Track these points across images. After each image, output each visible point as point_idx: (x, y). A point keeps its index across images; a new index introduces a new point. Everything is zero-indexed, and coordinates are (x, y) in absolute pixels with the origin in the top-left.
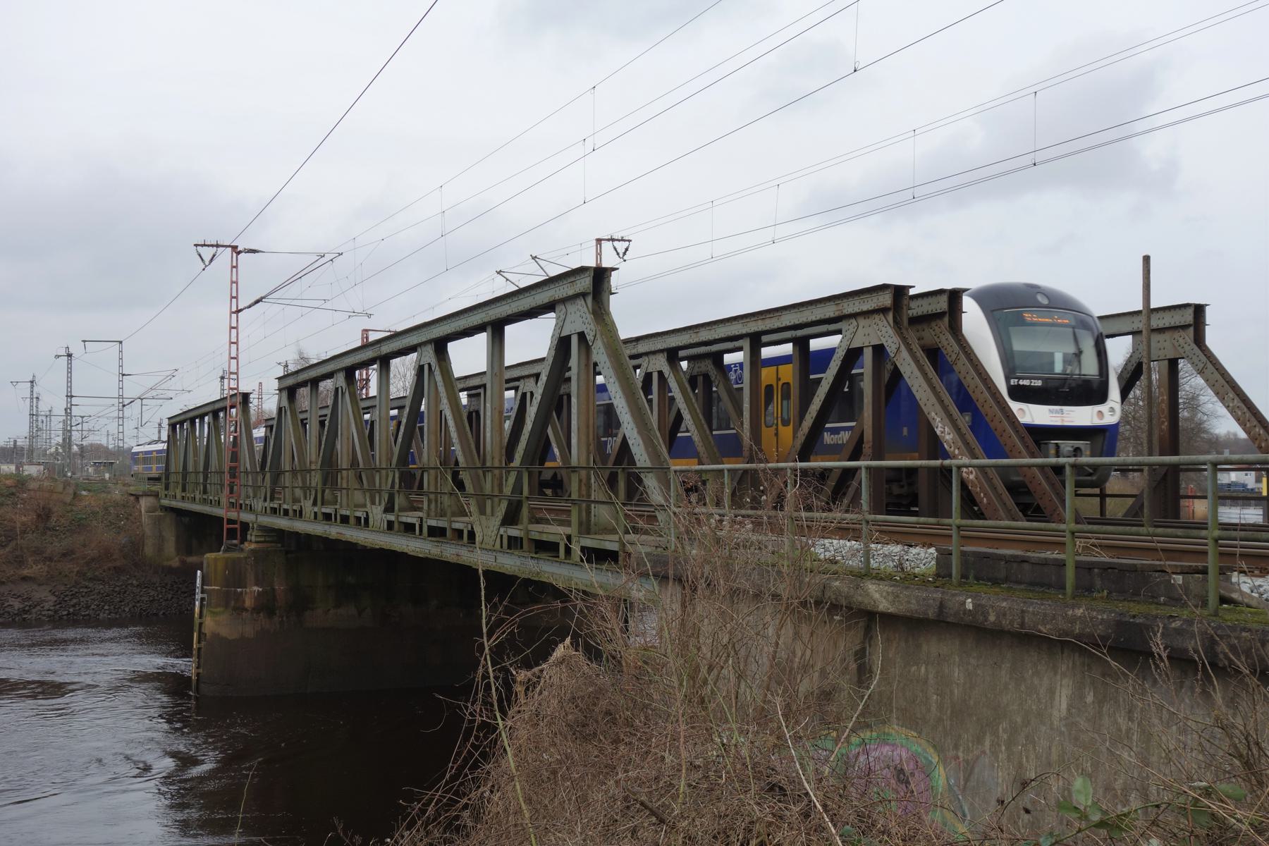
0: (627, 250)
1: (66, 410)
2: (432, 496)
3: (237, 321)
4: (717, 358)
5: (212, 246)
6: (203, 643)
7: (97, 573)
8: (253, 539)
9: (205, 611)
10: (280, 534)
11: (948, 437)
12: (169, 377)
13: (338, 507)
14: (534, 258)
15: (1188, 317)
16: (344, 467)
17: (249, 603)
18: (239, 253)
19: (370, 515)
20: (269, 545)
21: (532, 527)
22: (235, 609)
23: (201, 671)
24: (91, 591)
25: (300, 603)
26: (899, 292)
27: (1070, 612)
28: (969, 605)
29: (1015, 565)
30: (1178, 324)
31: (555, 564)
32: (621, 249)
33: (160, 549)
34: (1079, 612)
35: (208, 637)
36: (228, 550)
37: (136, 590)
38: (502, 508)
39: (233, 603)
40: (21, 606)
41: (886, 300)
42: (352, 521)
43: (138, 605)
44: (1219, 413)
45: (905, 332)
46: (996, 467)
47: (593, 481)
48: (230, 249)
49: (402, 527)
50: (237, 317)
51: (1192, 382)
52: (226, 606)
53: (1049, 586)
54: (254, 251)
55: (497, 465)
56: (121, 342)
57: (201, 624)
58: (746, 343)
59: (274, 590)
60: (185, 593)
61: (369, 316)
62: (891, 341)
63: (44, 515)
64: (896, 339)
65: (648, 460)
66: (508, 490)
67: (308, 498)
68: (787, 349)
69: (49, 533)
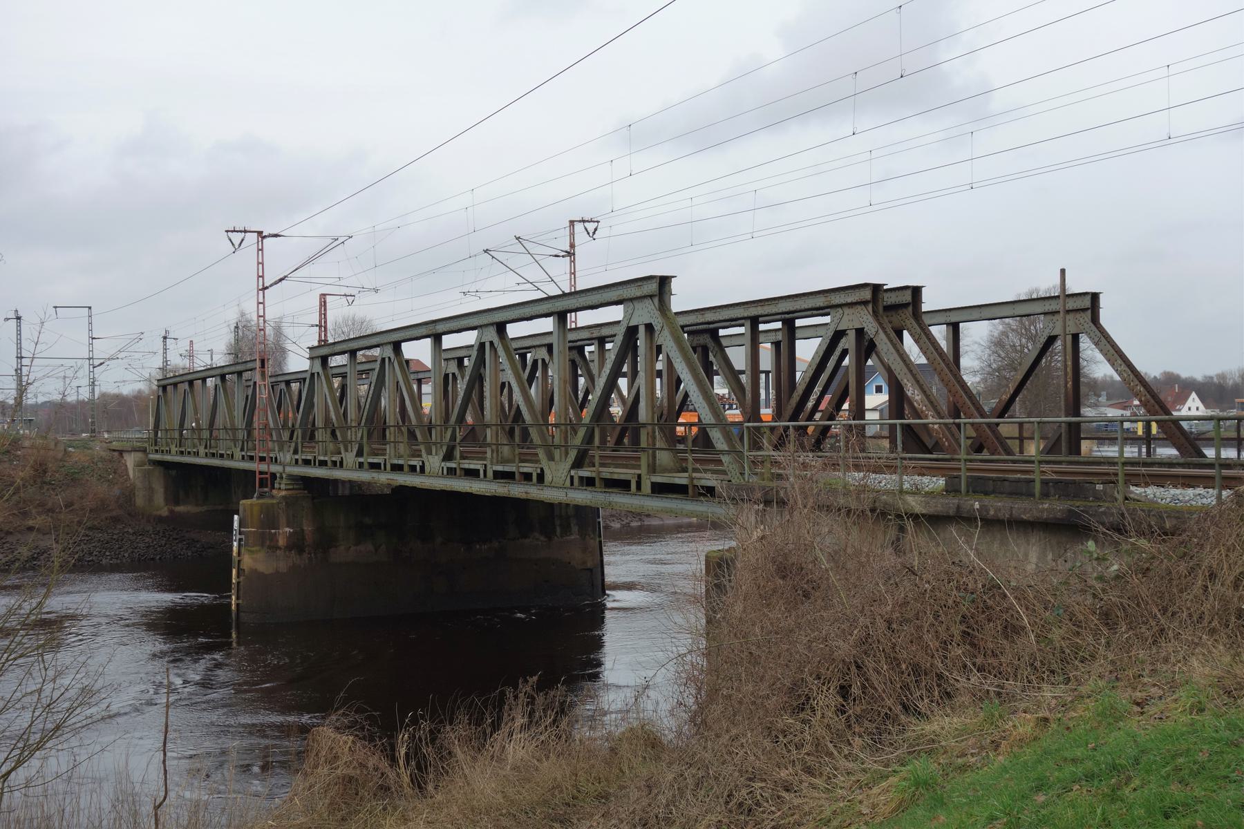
0: (596, 230)
1: (16, 370)
2: (494, 447)
3: (264, 297)
4: (716, 331)
5: (241, 231)
6: (242, 579)
7: (96, 523)
8: (283, 486)
9: (243, 550)
10: (306, 482)
11: (917, 398)
12: (136, 340)
13: (387, 457)
14: (518, 238)
15: (1087, 302)
16: (320, 426)
17: (282, 542)
18: (265, 237)
19: (427, 464)
20: (297, 492)
21: (601, 469)
22: (269, 547)
23: (240, 601)
24: (92, 539)
25: (326, 541)
26: (876, 289)
27: (1041, 507)
28: (977, 505)
29: (999, 483)
30: (1079, 307)
31: (626, 496)
32: (591, 229)
33: (150, 499)
34: (1046, 506)
35: (246, 572)
36: (261, 496)
37: (132, 538)
38: (573, 454)
39: (268, 543)
40: (31, 554)
41: (867, 295)
42: (406, 468)
43: (136, 551)
44: (1098, 359)
45: (880, 318)
46: (986, 424)
47: (657, 433)
48: (256, 234)
49: (463, 472)
50: (264, 294)
51: (1087, 347)
52: (262, 545)
53: (1022, 494)
54: (276, 236)
55: (563, 422)
56: (90, 308)
57: (239, 561)
58: (748, 323)
59: (303, 530)
60: (176, 539)
61: (376, 291)
62: (871, 327)
63: (41, 470)
64: (875, 324)
65: (712, 418)
66: (359, 439)
67: (350, 450)
68: (778, 325)
69: (46, 487)
